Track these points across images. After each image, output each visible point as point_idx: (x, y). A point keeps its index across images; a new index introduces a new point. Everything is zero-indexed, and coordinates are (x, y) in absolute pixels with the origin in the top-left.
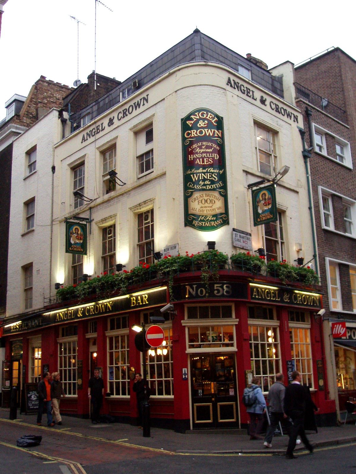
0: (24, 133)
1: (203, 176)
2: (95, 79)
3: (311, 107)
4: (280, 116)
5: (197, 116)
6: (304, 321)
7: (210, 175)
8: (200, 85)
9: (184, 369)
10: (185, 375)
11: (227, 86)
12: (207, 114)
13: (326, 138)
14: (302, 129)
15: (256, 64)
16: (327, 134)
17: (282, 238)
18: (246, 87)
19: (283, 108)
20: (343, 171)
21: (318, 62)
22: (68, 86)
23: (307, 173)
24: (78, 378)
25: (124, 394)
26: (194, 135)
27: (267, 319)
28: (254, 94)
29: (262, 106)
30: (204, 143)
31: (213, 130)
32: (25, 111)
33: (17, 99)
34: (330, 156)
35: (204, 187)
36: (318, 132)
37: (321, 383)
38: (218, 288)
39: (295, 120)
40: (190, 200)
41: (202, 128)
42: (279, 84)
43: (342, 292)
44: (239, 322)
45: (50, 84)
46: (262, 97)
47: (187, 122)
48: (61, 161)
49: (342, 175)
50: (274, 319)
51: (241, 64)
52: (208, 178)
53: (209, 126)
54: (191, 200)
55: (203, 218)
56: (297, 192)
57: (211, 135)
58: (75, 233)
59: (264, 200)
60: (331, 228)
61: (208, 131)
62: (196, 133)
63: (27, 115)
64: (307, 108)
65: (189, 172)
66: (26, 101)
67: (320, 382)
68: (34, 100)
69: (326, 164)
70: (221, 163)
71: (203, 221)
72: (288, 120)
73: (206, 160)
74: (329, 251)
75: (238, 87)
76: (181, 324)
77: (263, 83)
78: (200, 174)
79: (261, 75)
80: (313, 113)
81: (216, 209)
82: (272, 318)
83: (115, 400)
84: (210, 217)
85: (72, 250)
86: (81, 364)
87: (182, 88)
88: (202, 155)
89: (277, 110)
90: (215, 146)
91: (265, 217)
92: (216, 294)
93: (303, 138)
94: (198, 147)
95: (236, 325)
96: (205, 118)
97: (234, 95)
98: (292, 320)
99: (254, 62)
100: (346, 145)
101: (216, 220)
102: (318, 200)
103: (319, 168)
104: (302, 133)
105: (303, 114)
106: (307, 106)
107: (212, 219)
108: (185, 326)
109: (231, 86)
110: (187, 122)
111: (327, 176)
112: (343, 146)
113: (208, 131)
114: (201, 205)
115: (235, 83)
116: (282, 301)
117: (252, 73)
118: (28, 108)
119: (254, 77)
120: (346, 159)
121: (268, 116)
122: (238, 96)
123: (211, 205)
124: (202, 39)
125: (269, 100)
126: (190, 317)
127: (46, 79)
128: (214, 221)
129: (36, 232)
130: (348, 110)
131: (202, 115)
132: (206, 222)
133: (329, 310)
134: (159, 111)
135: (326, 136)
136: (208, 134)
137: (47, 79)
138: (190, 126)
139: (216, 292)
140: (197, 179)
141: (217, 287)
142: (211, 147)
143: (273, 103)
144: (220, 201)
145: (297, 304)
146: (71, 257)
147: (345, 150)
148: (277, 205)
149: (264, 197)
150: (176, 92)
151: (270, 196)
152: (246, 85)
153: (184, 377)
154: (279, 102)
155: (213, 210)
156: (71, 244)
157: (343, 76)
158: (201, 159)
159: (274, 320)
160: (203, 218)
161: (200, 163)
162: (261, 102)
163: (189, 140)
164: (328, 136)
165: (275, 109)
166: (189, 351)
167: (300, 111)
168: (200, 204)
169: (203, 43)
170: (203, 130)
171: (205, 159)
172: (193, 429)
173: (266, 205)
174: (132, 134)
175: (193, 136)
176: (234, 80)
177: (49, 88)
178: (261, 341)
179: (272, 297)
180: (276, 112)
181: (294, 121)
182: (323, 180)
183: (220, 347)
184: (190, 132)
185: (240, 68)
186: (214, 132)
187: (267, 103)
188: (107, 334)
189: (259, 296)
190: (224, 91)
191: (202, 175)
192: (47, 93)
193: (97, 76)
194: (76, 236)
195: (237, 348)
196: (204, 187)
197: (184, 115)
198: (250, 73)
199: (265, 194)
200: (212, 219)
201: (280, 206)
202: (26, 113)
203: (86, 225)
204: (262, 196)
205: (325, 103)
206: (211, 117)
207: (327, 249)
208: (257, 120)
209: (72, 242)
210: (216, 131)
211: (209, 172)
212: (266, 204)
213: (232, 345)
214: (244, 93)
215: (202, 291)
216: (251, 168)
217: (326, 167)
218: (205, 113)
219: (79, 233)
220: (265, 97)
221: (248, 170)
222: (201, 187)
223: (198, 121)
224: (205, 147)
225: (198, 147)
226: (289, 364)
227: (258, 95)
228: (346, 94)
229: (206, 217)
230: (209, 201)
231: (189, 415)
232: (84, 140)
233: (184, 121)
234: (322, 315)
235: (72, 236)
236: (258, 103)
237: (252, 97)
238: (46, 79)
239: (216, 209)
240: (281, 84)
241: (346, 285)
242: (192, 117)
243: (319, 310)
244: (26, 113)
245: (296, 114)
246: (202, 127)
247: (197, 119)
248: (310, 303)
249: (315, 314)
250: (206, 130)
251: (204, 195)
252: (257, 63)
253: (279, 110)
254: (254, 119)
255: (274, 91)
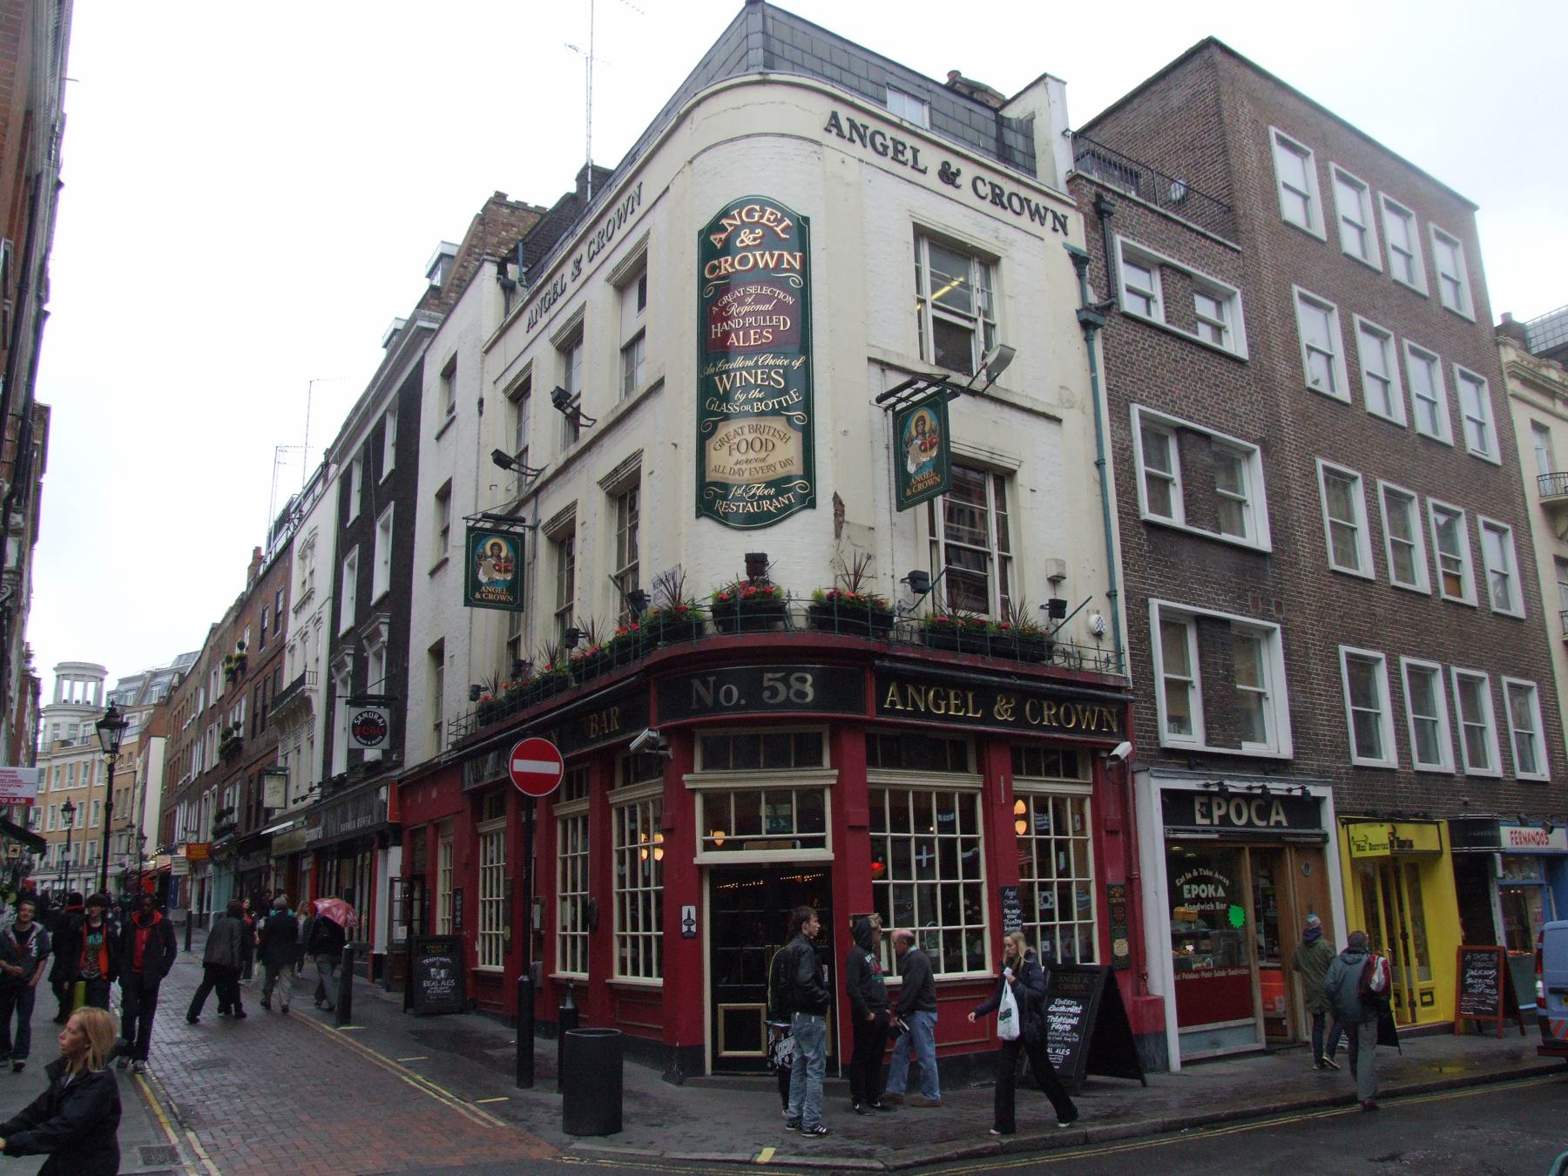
0: (441, 327)
1: (751, 377)
2: (590, 179)
3: (1114, 192)
4: (1008, 215)
5: (735, 219)
6: (1076, 776)
7: (762, 373)
8: (748, 136)
9: (685, 909)
10: (689, 925)
11: (827, 134)
12: (763, 211)
13: (1162, 276)
14: (1081, 251)
15: (970, 98)
16: (1163, 266)
17: (1004, 544)
18: (892, 139)
19: (1017, 195)
20: (1216, 367)
21: (1162, 85)
22: (526, 204)
23: (1093, 368)
24: (504, 927)
25: (648, 973)
26: (726, 269)
27: (946, 769)
28: (919, 156)
29: (948, 190)
30: (752, 289)
31: (776, 253)
32: (454, 278)
33: (446, 252)
34: (1174, 324)
35: (747, 408)
36: (1134, 259)
37: (1121, 948)
38: (771, 683)
39: (1058, 227)
40: (711, 444)
41: (747, 248)
42: (1020, 139)
43: (1204, 695)
44: (839, 778)
45: (517, 208)
46: (946, 164)
47: (712, 238)
48: (495, 383)
49: (1212, 375)
50: (970, 769)
51: (895, 84)
52: (759, 382)
53: (769, 240)
54: (712, 448)
55: (740, 492)
56: (1059, 421)
57: (771, 265)
58: (491, 556)
59: (920, 437)
60: (1177, 519)
61: (762, 256)
62: (732, 265)
63: (457, 286)
64: (1099, 197)
65: (711, 370)
66: (458, 253)
67: (1116, 946)
68: (477, 250)
69: (1158, 345)
70: (805, 348)
71: (741, 499)
72: (1035, 227)
73: (755, 333)
74: (1161, 582)
75: (862, 138)
76: (682, 783)
77: (970, 134)
78: (738, 374)
79: (965, 117)
80: (1119, 207)
81: (778, 467)
82: (961, 767)
83: (636, 989)
84: (758, 488)
85: (481, 600)
86: (1121, 896)
87: (704, 151)
88: (744, 320)
89: (997, 198)
90: (781, 296)
91: (921, 482)
92: (767, 700)
93: (1080, 276)
94: (734, 300)
95: (831, 786)
96: (754, 223)
97: (847, 159)
98: (1017, 770)
99: (965, 91)
100: (1230, 296)
101: (776, 496)
102: (1131, 441)
103: (1134, 357)
104: (1078, 260)
105: (1087, 210)
106: (1100, 190)
107: (766, 493)
108: (693, 791)
109: (840, 134)
110: (712, 238)
111: (1163, 379)
112: (1219, 298)
113: (762, 256)
114: (737, 456)
115: (853, 125)
116: (988, 719)
117: (931, 109)
118: (462, 270)
119: (939, 120)
120: (1231, 332)
121: (965, 216)
122: (860, 160)
123: (763, 454)
124: (769, 22)
125: (968, 172)
126: (707, 765)
127: (508, 199)
128: (769, 497)
129: (450, 563)
130: (1239, 204)
131: (749, 214)
132: (747, 502)
133: (1158, 744)
134: (657, 221)
135: (1161, 271)
136: (761, 265)
137: (511, 199)
138: (719, 246)
139: (767, 694)
140: (728, 388)
141: (770, 680)
142: (768, 299)
143: (983, 180)
144: (791, 442)
145: (1040, 727)
146: (508, 617)
147: (1226, 308)
148: (952, 444)
149: (920, 429)
150: (691, 162)
151: (935, 423)
152: (890, 132)
153: (685, 929)
154: (1005, 180)
155: (769, 467)
156: (480, 584)
157: (1225, 114)
158: (741, 333)
159: (968, 772)
160: (740, 492)
161: (738, 342)
162: (942, 180)
163: (715, 286)
164: (1168, 272)
165: (990, 197)
166: (704, 857)
167: (1075, 204)
168: (735, 453)
169: (771, 32)
170: (750, 255)
171: (752, 332)
172: (713, 1074)
173: (925, 450)
174: (610, 290)
175: (723, 272)
176: (852, 117)
177: (513, 220)
178: (892, 831)
179: (953, 707)
180: (994, 207)
181: (1055, 230)
182: (1149, 388)
183: (794, 847)
184: (716, 262)
185: (891, 97)
186: (781, 256)
187: (965, 180)
188: (557, 813)
189: (905, 704)
190: (816, 147)
191: (741, 374)
192: (507, 231)
193: (592, 171)
194: (494, 562)
195: (834, 851)
196: (747, 408)
197: (704, 221)
198: (926, 109)
199: (922, 419)
200: (766, 493)
201: (994, 456)
202: (456, 282)
203: (522, 536)
204: (916, 426)
205: (1177, 192)
206: (772, 218)
207: (1157, 577)
208: (923, 224)
209: (483, 578)
210: (786, 255)
211: (763, 367)
212: (924, 449)
213: (819, 843)
214: (884, 154)
215: (729, 694)
216: (898, 354)
217: (1159, 355)
218: (758, 208)
219: (503, 554)
220: (956, 163)
221: (886, 359)
222: (739, 406)
223: (737, 229)
224: (753, 301)
225: (734, 300)
226: (1008, 898)
227: (932, 159)
228: (1232, 161)
229: (748, 487)
230: (757, 445)
231: (702, 1038)
232: (531, 325)
233: (705, 235)
234: (1123, 757)
235: (483, 563)
236: (932, 179)
237: (911, 162)
238: (508, 199)
239: (778, 467)
240: (1028, 136)
241: (1218, 674)
242: (725, 222)
243: (1116, 745)
244: (456, 282)
245: (1060, 210)
246: (748, 246)
247: (736, 226)
248: (1088, 725)
249: (1104, 755)
250: (758, 254)
251: (746, 430)
252: (972, 93)
253: (1005, 200)
254: (914, 223)
255: (1004, 153)
